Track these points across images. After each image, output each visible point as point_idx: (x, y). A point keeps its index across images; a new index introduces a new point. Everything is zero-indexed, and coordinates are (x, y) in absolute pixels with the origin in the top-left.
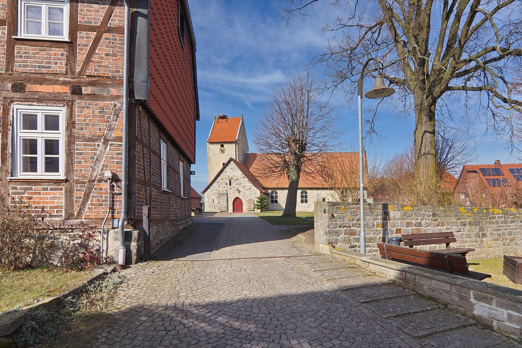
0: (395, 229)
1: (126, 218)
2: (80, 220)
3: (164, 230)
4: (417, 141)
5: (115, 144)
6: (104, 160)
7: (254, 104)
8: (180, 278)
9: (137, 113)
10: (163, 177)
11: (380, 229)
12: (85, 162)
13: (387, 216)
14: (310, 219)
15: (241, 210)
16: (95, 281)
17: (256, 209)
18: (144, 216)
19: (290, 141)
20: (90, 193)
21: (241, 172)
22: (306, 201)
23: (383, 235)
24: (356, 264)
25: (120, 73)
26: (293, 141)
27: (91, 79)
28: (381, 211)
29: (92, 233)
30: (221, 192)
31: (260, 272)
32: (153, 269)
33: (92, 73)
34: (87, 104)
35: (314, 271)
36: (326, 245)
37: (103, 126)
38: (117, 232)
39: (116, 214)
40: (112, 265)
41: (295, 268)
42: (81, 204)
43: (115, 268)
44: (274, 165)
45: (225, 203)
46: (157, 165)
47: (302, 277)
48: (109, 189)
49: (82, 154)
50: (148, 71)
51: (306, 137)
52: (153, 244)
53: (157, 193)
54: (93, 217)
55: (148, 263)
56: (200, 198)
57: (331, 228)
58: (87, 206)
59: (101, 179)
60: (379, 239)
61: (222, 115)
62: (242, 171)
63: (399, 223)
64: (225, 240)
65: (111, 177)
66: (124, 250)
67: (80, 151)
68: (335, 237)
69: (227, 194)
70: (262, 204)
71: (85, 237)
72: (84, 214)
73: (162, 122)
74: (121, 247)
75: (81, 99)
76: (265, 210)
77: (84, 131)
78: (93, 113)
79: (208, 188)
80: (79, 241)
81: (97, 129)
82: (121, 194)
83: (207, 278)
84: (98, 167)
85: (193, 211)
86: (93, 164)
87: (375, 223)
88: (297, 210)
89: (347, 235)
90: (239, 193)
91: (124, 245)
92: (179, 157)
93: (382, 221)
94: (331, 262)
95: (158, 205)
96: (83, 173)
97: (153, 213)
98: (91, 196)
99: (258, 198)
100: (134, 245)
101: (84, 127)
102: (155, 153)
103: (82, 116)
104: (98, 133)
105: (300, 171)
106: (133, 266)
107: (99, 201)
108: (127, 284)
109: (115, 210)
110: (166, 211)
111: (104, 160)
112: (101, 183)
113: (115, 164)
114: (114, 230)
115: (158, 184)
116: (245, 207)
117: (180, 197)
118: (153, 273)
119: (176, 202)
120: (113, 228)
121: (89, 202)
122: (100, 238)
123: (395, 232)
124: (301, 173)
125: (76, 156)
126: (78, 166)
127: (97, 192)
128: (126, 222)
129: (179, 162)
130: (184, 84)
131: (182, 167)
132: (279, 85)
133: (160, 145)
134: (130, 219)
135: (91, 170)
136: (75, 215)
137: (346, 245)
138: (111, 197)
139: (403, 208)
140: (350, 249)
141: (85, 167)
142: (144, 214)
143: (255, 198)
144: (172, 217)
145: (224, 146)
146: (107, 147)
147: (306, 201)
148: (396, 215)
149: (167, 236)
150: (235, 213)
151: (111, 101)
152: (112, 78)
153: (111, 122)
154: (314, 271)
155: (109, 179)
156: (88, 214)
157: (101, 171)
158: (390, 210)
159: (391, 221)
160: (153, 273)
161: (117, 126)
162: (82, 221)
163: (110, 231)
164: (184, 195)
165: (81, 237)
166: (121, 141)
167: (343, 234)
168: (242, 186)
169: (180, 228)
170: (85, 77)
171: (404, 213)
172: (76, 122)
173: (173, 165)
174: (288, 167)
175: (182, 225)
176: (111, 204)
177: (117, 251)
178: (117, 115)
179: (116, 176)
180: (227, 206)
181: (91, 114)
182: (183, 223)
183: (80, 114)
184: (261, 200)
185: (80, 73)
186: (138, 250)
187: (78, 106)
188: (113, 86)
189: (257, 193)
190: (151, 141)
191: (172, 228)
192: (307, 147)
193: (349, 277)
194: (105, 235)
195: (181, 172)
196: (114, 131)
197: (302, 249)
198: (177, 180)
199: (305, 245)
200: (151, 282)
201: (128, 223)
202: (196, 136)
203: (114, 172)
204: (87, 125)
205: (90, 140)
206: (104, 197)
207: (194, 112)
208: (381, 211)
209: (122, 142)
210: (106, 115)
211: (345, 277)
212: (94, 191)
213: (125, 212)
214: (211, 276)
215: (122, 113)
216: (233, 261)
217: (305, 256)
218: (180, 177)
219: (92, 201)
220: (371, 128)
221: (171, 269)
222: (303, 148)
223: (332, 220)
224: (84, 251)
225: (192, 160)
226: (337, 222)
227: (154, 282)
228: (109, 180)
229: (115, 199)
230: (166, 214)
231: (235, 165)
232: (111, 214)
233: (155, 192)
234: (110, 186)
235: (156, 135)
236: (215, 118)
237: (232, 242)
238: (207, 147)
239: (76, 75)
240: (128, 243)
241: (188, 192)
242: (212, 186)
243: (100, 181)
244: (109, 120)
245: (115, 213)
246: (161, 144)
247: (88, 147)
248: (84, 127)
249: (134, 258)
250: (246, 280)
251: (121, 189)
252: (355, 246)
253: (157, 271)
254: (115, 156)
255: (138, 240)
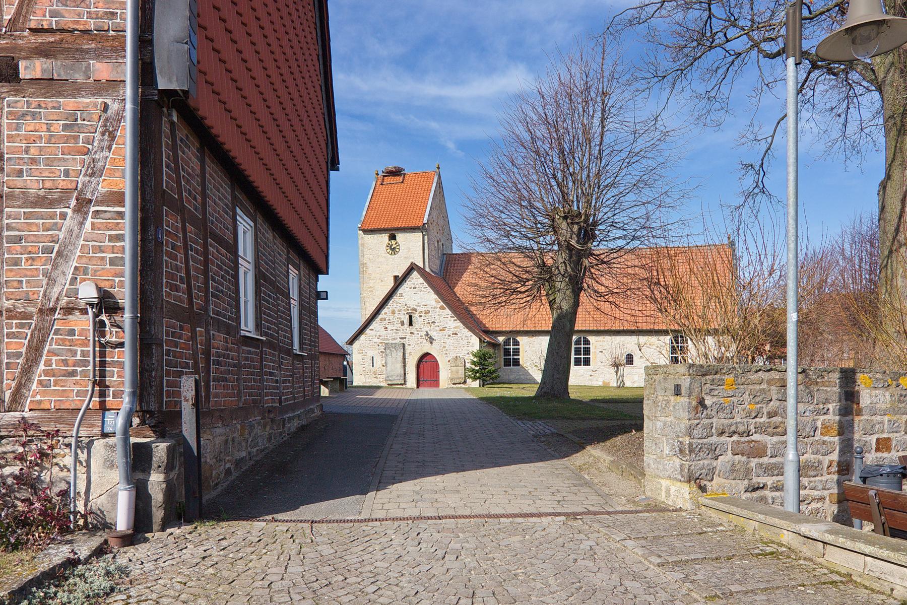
0: (873, 439)
1: (138, 408)
2: (17, 414)
3: (247, 436)
4: (888, 208)
5: (106, 211)
6: (78, 254)
7: (465, 145)
8: (274, 578)
9: (166, 129)
10: (246, 302)
11: (831, 439)
12: (30, 262)
13: (853, 402)
14: (602, 405)
15: (435, 382)
16: (34, 589)
17: (469, 381)
18: (183, 403)
19: (557, 217)
20: (43, 342)
21: (436, 297)
22: (587, 362)
23: (840, 456)
24: (780, 545)
25: (119, 20)
26: (565, 218)
27: (42, 39)
28: (835, 389)
29: (48, 449)
30: (391, 342)
31: (499, 563)
32: (205, 548)
33: (44, 23)
34: (33, 106)
35: (661, 565)
36: (679, 484)
37: (76, 163)
38: (112, 447)
39: (111, 398)
40: (99, 534)
41: (600, 552)
42: (20, 373)
43: (106, 542)
44: (516, 276)
45: (399, 365)
46: (227, 272)
47: (627, 583)
48: (91, 331)
49: (21, 240)
50: (191, 11)
51: (595, 206)
52: (214, 472)
53: (227, 342)
54: (53, 407)
55: (196, 528)
56: (344, 355)
57: (697, 436)
58: (37, 378)
59: (71, 306)
60: (828, 467)
61: (391, 167)
62: (437, 292)
63: (886, 424)
64: (399, 462)
65: (96, 301)
66: (130, 494)
67: (17, 233)
68: (706, 462)
69: (404, 345)
70: (485, 369)
71: (29, 458)
72: (29, 399)
73: (279, 215)
74: (123, 486)
75: (17, 92)
76: (491, 381)
77: (25, 178)
78: (49, 130)
79: (361, 332)
80: (16, 470)
81: (58, 173)
82: (122, 345)
83: (351, 580)
84: (64, 273)
85: (325, 384)
86: (50, 267)
87: (819, 424)
88: (570, 383)
89: (740, 456)
90: (431, 343)
91: (129, 479)
92: (287, 255)
93: (837, 418)
94: (700, 534)
95: (229, 372)
96: (25, 289)
97: (216, 396)
98: (45, 352)
99: (475, 356)
100: (156, 480)
101: (24, 168)
102: (220, 241)
103: (18, 139)
104: (63, 182)
105: (581, 289)
106: (155, 535)
107: (65, 362)
108: (125, 597)
109: (108, 387)
110: (252, 388)
111: (78, 254)
112: (70, 317)
113: (108, 266)
114: (107, 440)
115: (230, 318)
116: (444, 375)
117: (289, 352)
118: (204, 558)
119: (281, 364)
120: (105, 435)
121: (42, 367)
122: (68, 461)
123: (874, 446)
124: (581, 294)
125: (5, 245)
126: (11, 270)
127: (61, 339)
128: (138, 419)
129: (288, 268)
130: (297, 75)
131: (296, 281)
132: (521, 97)
133: (235, 221)
134: (148, 412)
135: (44, 283)
136: (6, 400)
137: (737, 484)
138: (97, 354)
139: (897, 380)
140: (748, 495)
141: (29, 273)
142: (185, 397)
143: (468, 354)
144: (269, 401)
145: (397, 238)
146: (85, 219)
147: (587, 362)
148: (877, 400)
149: (255, 450)
150: (421, 389)
151: (93, 95)
152: (96, 35)
153: (95, 153)
154: (661, 565)
155: (92, 305)
156: (38, 398)
157: (71, 284)
158: (862, 386)
159: (862, 418)
160: (204, 558)
161: (112, 164)
162: (23, 418)
163: (95, 442)
164: (301, 348)
165: (21, 458)
166: (121, 203)
167: (729, 452)
168: (437, 328)
169: (289, 428)
170: (25, 33)
171: (901, 395)
172: (6, 156)
173: (271, 274)
174: (550, 280)
175: (296, 420)
176: (97, 373)
177: (114, 497)
178: (110, 133)
179: (109, 298)
180: (403, 372)
181: (42, 134)
182: (298, 416)
183: (13, 133)
184: (482, 358)
185: (13, 22)
186: (170, 492)
187: (9, 113)
188: (99, 55)
189: (474, 343)
190: (209, 209)
191: (268, 428)
192: (599, 230)
193: (773, 587)
194: (82, 452)
195: (294, 293)
196: (103, 177)
197: (606, 490)
198: (283, 313)
199: (612, 478)
200: (192, 590)
201: (143, 422)
202: (331, 208)
203: (105, 285)
204: (33, 161)
205: (41, 201)
206: (79, 353)
207: (324, 150)
208: (837, 389)
209: (124, 206)
210: (82, 135)
211: (761, 590)
212: (55, 337)
213: (133, 394)
214: (361, 573)
215: (124, 128)
216: (423, 525)
217: (623, 512)
218: (289, 304)
219: (48, 363)
220: (757, 183)
221: (253, 549)
222: (587, 233)
223: (699, 415)
224: (28, 496)
225: (322, 265)
226: (714, 420)
227: (200, 591)
228: (92, 308)
229: (107, 359)
230: (250, 395)
231: (421, 280)
232: (97, 399)
233: (219, 340)
234: (95, 323)
235: (223, 194)
236: (377, 174)
237: (417, 467)
238: (360, 242)
239: (4, 30)
240: (140, 476)
241: (311, 341)
242: (371, 328)
243: (68, 310)
244: (90, 147)
245: (109, 396)
246: (238, 218)
247: (37, 221)
248: (24, 168)
249: (158, 515)
250: (463, 590)
251: (124, 332)
252: (762, 488)
253: (214, 552)
254: (107, 243)
255: (169, 468)
